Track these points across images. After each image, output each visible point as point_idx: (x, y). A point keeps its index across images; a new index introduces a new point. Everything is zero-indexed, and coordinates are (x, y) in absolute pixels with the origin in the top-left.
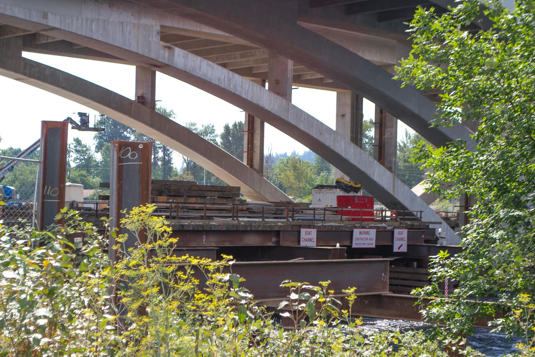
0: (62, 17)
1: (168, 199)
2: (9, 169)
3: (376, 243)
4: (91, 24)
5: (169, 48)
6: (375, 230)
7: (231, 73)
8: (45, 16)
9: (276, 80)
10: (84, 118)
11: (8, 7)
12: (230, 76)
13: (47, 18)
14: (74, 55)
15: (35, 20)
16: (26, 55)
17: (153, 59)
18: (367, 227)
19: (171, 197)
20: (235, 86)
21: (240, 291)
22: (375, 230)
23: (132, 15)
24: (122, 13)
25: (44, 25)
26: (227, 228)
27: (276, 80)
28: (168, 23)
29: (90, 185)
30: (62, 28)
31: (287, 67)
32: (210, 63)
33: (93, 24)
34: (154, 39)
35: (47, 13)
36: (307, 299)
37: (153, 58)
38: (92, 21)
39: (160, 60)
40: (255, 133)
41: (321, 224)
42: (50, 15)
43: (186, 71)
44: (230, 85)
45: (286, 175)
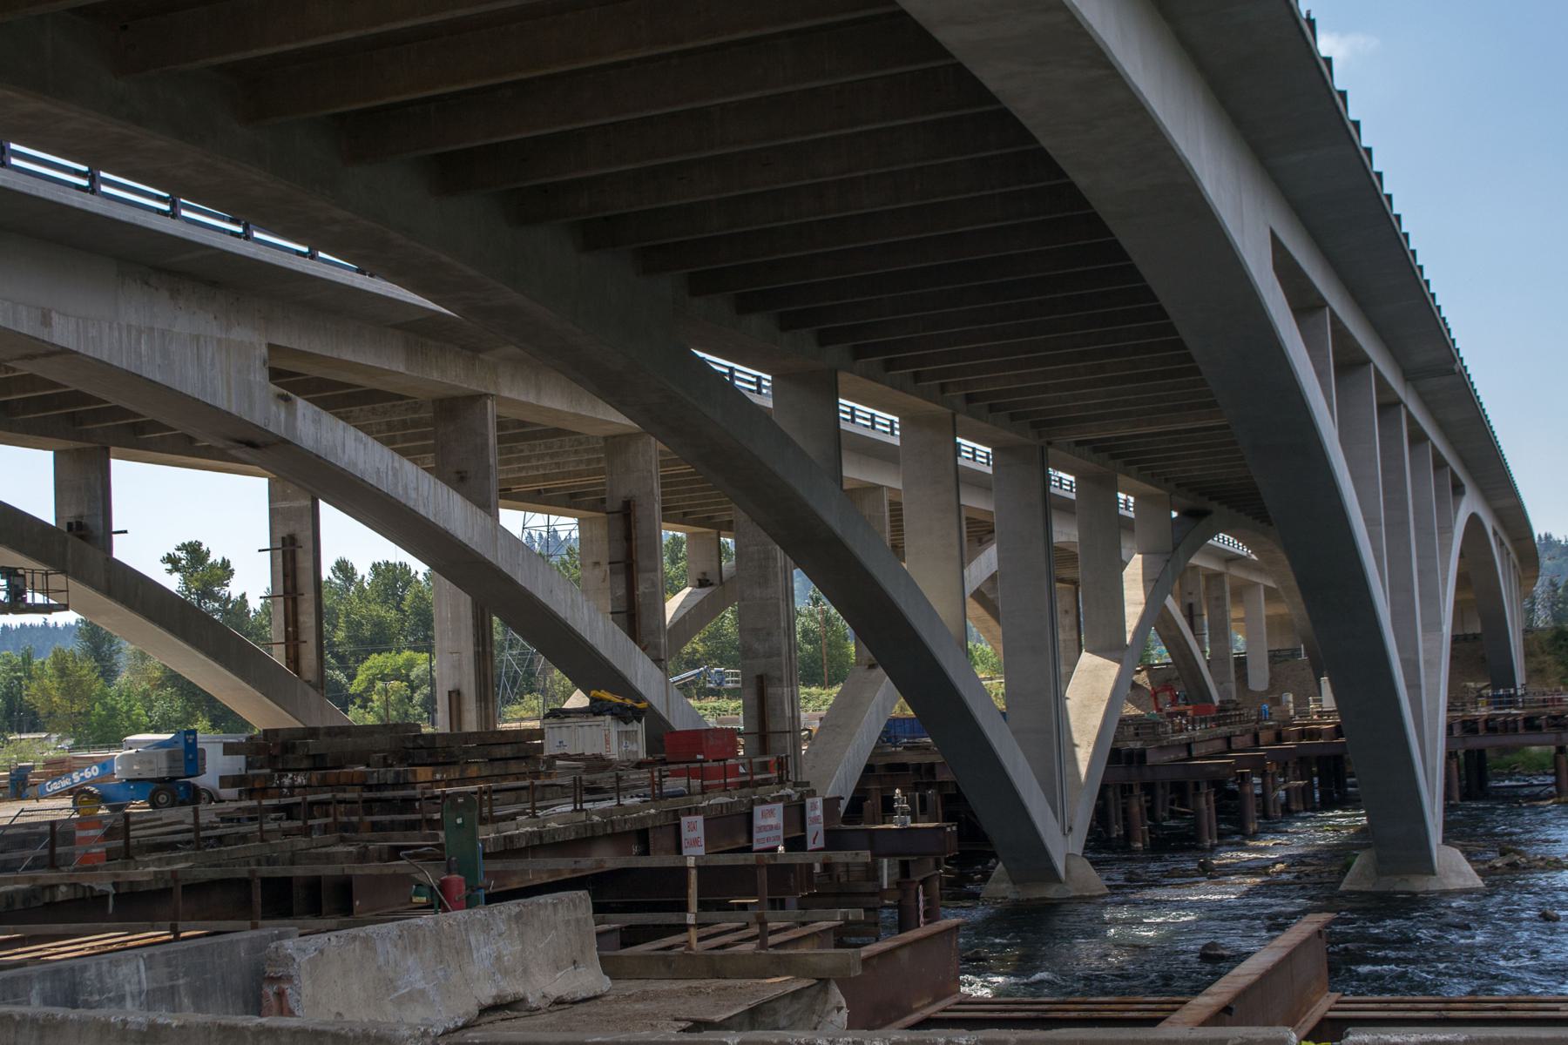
0: (80, 321)
1: (434, 774)
3: (784, 834)
4: (138, 341)
5: (286, 399)
6: (781, 805)
7: (397, 456)
8: (46, 321)
10: (17, 581)
12: (397, 465)
13: (51, 325)
15: (25, 331)
17: (258, 427)
18: (768, 799)
19: (440, 768)
20: (406, 488)
21: (144, 959)
22: (781, 805)
23: (215, 318)
24: (194, 313)
25: (44, 341)
26: (577, 833)
27: (458, 473)
28: (281, 340)
30: (82, 351)
31: (487, 440)
32: (361, 434)
33: (143, 341)
34: (258, 379)
35: (50, 311)
36: (1222, 1014)
37: (259, 424)
38: (140, 332)
40: (300, 598)
41: (614, 803)
42: (55, 317)
43: (320, 454)
44: (396, 485)
45: (44, 690)
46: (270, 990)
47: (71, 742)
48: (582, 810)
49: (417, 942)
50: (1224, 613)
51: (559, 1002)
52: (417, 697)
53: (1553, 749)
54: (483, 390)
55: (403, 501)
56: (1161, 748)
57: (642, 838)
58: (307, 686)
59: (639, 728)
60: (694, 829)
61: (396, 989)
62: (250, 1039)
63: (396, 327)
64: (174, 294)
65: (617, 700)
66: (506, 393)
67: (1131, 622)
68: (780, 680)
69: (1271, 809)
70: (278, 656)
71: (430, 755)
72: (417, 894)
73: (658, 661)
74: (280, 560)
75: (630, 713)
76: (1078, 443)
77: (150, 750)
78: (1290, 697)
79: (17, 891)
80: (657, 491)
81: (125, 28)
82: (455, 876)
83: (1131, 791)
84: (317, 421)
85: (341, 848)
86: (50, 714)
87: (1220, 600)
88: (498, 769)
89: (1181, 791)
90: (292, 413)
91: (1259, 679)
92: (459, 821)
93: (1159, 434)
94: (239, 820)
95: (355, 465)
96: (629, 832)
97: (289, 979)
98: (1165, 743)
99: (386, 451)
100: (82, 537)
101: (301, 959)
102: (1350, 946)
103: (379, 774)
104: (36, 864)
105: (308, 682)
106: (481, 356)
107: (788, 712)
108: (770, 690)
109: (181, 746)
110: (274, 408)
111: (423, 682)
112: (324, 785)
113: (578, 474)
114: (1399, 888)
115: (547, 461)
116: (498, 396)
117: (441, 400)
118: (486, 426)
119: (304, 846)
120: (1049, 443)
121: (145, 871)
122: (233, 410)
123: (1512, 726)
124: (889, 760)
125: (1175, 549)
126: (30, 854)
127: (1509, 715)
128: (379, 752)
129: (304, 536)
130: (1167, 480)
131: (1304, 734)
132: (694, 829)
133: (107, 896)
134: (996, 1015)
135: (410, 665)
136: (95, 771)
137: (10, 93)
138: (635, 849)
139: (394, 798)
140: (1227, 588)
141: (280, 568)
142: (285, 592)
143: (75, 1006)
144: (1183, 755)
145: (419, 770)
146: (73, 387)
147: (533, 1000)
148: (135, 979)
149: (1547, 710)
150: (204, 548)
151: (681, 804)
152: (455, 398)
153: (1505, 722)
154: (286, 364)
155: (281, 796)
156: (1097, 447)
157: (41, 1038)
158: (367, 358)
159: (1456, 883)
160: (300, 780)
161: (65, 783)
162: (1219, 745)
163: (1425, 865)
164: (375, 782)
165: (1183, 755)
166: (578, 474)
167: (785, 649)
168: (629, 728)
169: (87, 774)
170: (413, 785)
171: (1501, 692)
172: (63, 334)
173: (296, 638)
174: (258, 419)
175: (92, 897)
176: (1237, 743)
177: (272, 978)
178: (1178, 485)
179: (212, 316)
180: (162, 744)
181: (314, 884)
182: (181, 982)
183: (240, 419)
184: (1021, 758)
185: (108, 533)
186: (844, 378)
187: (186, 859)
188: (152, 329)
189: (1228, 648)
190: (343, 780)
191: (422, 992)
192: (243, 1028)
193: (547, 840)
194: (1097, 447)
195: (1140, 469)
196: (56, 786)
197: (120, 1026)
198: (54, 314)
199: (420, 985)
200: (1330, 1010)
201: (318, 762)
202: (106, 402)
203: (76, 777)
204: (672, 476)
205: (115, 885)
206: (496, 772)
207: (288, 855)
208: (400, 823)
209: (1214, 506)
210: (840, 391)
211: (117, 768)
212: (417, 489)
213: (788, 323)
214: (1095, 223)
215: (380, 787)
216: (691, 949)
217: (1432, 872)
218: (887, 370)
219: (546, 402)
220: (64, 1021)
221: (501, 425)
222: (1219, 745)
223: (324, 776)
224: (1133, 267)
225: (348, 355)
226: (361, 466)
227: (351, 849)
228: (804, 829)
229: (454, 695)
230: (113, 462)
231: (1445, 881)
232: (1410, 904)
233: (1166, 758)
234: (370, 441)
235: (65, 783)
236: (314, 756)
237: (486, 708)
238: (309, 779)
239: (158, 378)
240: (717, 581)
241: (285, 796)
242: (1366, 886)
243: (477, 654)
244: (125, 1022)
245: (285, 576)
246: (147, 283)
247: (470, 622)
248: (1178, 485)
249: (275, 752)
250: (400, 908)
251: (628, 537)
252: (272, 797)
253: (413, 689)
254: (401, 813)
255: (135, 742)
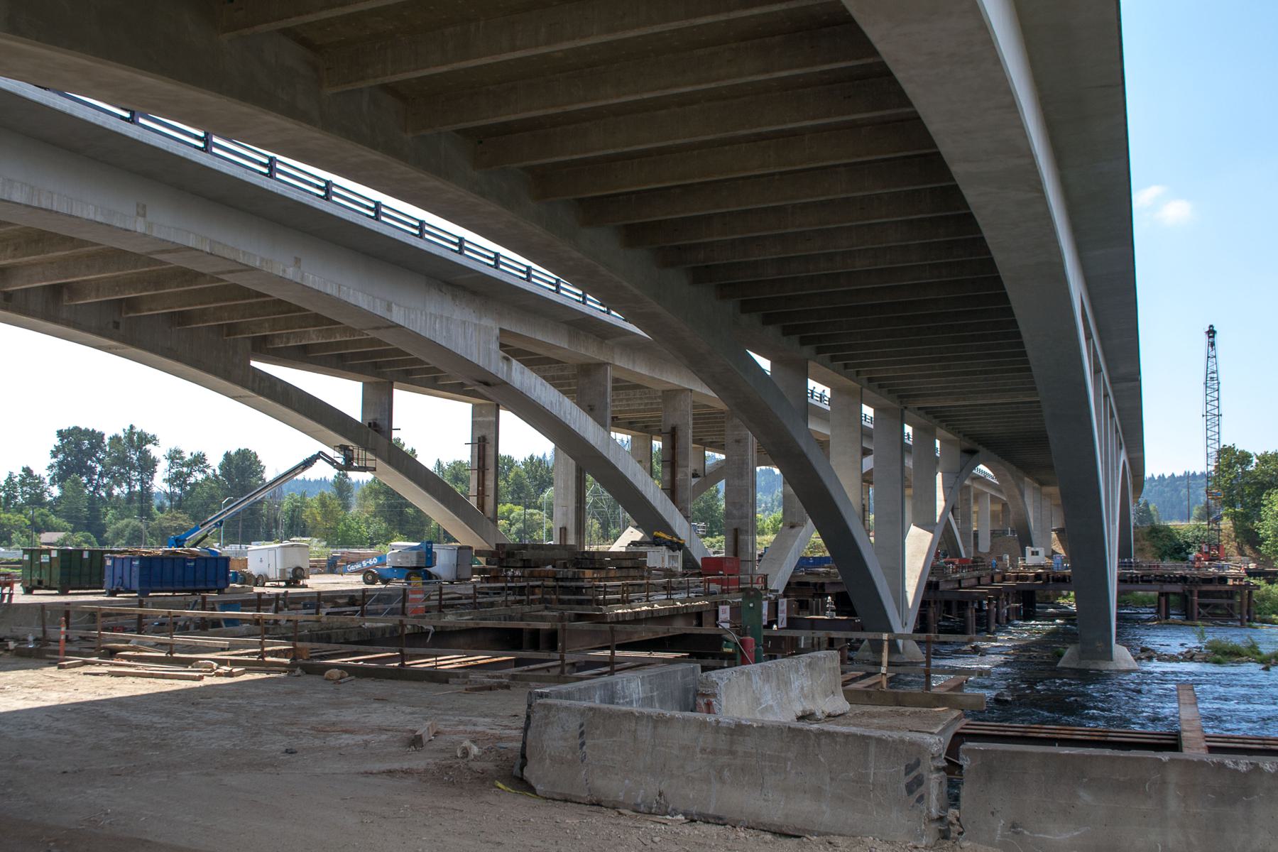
2: (216, 524)
5: (508, 359)
7: (561, 395)
8: (389, 309)
9: (589, 406)
11: (352, 291)
14: (306, 365)
15: (378, 314)
16: (254, 364)
19: (596, 571)
20: (565, 413)
27: (589, 406)
29: (52, 527)
32: (544, 381)
38: (436, 318)
39: (499, 376)
42: (394, 307)
44: (560, 411)
45: (312, 513)
46: (702, 702)
47: (325, 543)
48: (671, 599)
49: (769, 677)
50: (969, 508)
51: (829, 716)
52: (514, 529)
53: (1157, 593)
54: (606, 361)
55: (563, 420)
56: (947, 581)
57: (699, 616)
58: (489, 521)
59: (679, 554)
60: (725, 613)
61: (761, 704)
62: (813, 738)
63: (566, 323)
64: (454, 297)
65: (668, 538)
66: (617, 363)
67: (939, 511)
68: (747, 532)
69: (1001, 618)
70: (473, 502)
71: (591, 563)
72: (727, 647)
73: (686, 517)
74: (476, 450)
75: (676, 546)
76: (919, 409)
77: (407, 551)
78: (1008, 557)
79: (387, 627)
80: (691, 422)
81: (481, 142)
82: (749, 638)
83: (929, 604)
84: (522, 373)
85: (546, 613)
86: (314, 528)
87: (968, 500)
88: (624, 573)
89: (962, 605)
90: (510, 368)
91: (985, 546)
92: (751, 605)
93: (964, 406)
94: (487, 594)
95: (540, 398)
96: (692, 613)
97: (715, 695)
98: (949, 578)
99: (556, 392)
100: (376, 431)
101: (722, 684)
102: (1079, 699)
103: (562, 573)
104: (392, 612)
105: (489, 518)
106: (606, 341)
107: (750, 550)
108: (741, 537)
109: (425, 550)
110: (501, 364)
111: (517, 521)
112: (532, 576)
113: (638, 411)
114: (1091, 667)
115: (624, 402)
116: (614, 364)
117: (582, 365)
118: (607, 381)
119: (527, 610)
120: (906, 408)
121: (450, 619)
122: (481, 364)
123: (1135, 579)
124: (799, 580)
125: (961, 470)
126: (389, 607)
127: (1132, 573)
128: (561, 560)
129: (491, 437)
130: (959, 432)
131: (1017, 578)
132: (725, 613)
133: (428, 632)
134: (1096, 738)
135: (511, 511)
136: (375, 561)
137: (422, 175)
138: (694, 622)
139: (571, 587)
140: (972, 494)
141: (476, 454)
142: (479, 467)
143: (613, 703)
144: (957, 586)
145: (587, 571)
146: (396, 346)
147: (819, 715)
148: (637, 691)
149: (1154, 572)
150: (402, 442)
151: (718, 598)
152: (590, 364)
153: (1131, 577)
154: (507, 341)
155: (507, 582)
156: (928, 411)
157: (655, 727)
158: (550, 340)
159: (1124, 666)
160: (518, 573)
161: (358, 566)
162: (974, 581)
163: (1108, 655)
164: (561, 576)
165: (957, 586)
166: (638, 411)
167: (750, 514)
168: (674, 554)
169: (371, 562)
170: (582, 580)
171: (1126, 560)
172: (397, 316)
173: (483, 494)
174: (493, 370)
175: (423, 633)
176: (983, 581)
177: (704, 694)
178: (965, 435)
179: (472, 311)
180: (413, 548)
181: (536, 633)
182: (655, 694)
183: (484, 369)
184: (885, 582)
185: (390, 429)
186: (811, 364)
187: (469, 614)
188: (442, 316)
189: (970, 529)
190: (542, 574)
191: (771, 706)
192: (808, 731)
193: (655, 615)
194: (928, 411)
195: (947, 425)
196: (353, 568)
197: (714, 724)
198: (393, 305)
199: (770, 703)
200: (962, 728)
201: (526, 564)
202: (410, 355)
203: (364, 563)
204: (699, 414)
205: (434, 627)
206: (623, 575)
207: (519, 615)
208: (574, 600)
209: (980, 448)
210: (810, 371)
211: (388, 560)
212: (570, 414)
213: (787, 332)
214: (997, 281)
215: (562, 580)
216: (882, 688)
217: (1111, 660)
218: (832, 361)
219: (638, 370)
220: (672, 718)
221: (616, 380)
222: (974, 581)
223: (532, 572)
224: (1010, 309)
225: (539, 337)
226: (543, 398)
227: (555, 613)
228: (777, 616)
229: (563, 530)
230: (395, 391)
231: (1118, 665)
232: (1100, 677)
233: (948, 587)
234: (548, 385)
235: (358, 566)
236: (524, 560)
237: (580, 538)
238: (523, 573)
239: (444, 344)
240: (702, 475)
241: (509, 582)
242: (1073, 665)
243: (576, 507)
244: (718, 722)
245: (479, 458)
246: (441, 291)
247: (574, 490)
248: (965, 435)
249: (502, 556)
250: (581, 649)
251: (673, 447)
252: (502, 582)
253: (511, 525)
254: (574, 595)
255: (396, 546)
